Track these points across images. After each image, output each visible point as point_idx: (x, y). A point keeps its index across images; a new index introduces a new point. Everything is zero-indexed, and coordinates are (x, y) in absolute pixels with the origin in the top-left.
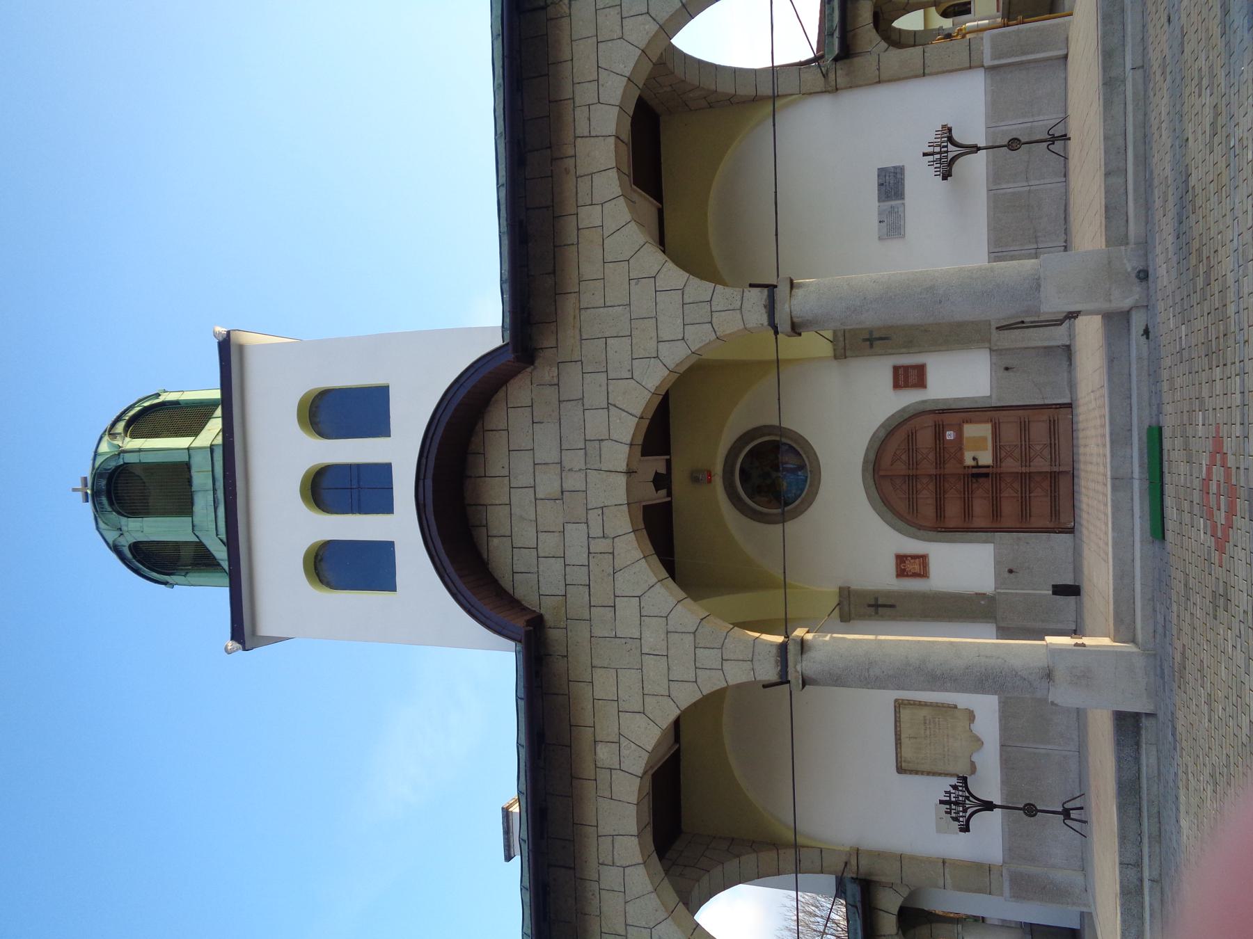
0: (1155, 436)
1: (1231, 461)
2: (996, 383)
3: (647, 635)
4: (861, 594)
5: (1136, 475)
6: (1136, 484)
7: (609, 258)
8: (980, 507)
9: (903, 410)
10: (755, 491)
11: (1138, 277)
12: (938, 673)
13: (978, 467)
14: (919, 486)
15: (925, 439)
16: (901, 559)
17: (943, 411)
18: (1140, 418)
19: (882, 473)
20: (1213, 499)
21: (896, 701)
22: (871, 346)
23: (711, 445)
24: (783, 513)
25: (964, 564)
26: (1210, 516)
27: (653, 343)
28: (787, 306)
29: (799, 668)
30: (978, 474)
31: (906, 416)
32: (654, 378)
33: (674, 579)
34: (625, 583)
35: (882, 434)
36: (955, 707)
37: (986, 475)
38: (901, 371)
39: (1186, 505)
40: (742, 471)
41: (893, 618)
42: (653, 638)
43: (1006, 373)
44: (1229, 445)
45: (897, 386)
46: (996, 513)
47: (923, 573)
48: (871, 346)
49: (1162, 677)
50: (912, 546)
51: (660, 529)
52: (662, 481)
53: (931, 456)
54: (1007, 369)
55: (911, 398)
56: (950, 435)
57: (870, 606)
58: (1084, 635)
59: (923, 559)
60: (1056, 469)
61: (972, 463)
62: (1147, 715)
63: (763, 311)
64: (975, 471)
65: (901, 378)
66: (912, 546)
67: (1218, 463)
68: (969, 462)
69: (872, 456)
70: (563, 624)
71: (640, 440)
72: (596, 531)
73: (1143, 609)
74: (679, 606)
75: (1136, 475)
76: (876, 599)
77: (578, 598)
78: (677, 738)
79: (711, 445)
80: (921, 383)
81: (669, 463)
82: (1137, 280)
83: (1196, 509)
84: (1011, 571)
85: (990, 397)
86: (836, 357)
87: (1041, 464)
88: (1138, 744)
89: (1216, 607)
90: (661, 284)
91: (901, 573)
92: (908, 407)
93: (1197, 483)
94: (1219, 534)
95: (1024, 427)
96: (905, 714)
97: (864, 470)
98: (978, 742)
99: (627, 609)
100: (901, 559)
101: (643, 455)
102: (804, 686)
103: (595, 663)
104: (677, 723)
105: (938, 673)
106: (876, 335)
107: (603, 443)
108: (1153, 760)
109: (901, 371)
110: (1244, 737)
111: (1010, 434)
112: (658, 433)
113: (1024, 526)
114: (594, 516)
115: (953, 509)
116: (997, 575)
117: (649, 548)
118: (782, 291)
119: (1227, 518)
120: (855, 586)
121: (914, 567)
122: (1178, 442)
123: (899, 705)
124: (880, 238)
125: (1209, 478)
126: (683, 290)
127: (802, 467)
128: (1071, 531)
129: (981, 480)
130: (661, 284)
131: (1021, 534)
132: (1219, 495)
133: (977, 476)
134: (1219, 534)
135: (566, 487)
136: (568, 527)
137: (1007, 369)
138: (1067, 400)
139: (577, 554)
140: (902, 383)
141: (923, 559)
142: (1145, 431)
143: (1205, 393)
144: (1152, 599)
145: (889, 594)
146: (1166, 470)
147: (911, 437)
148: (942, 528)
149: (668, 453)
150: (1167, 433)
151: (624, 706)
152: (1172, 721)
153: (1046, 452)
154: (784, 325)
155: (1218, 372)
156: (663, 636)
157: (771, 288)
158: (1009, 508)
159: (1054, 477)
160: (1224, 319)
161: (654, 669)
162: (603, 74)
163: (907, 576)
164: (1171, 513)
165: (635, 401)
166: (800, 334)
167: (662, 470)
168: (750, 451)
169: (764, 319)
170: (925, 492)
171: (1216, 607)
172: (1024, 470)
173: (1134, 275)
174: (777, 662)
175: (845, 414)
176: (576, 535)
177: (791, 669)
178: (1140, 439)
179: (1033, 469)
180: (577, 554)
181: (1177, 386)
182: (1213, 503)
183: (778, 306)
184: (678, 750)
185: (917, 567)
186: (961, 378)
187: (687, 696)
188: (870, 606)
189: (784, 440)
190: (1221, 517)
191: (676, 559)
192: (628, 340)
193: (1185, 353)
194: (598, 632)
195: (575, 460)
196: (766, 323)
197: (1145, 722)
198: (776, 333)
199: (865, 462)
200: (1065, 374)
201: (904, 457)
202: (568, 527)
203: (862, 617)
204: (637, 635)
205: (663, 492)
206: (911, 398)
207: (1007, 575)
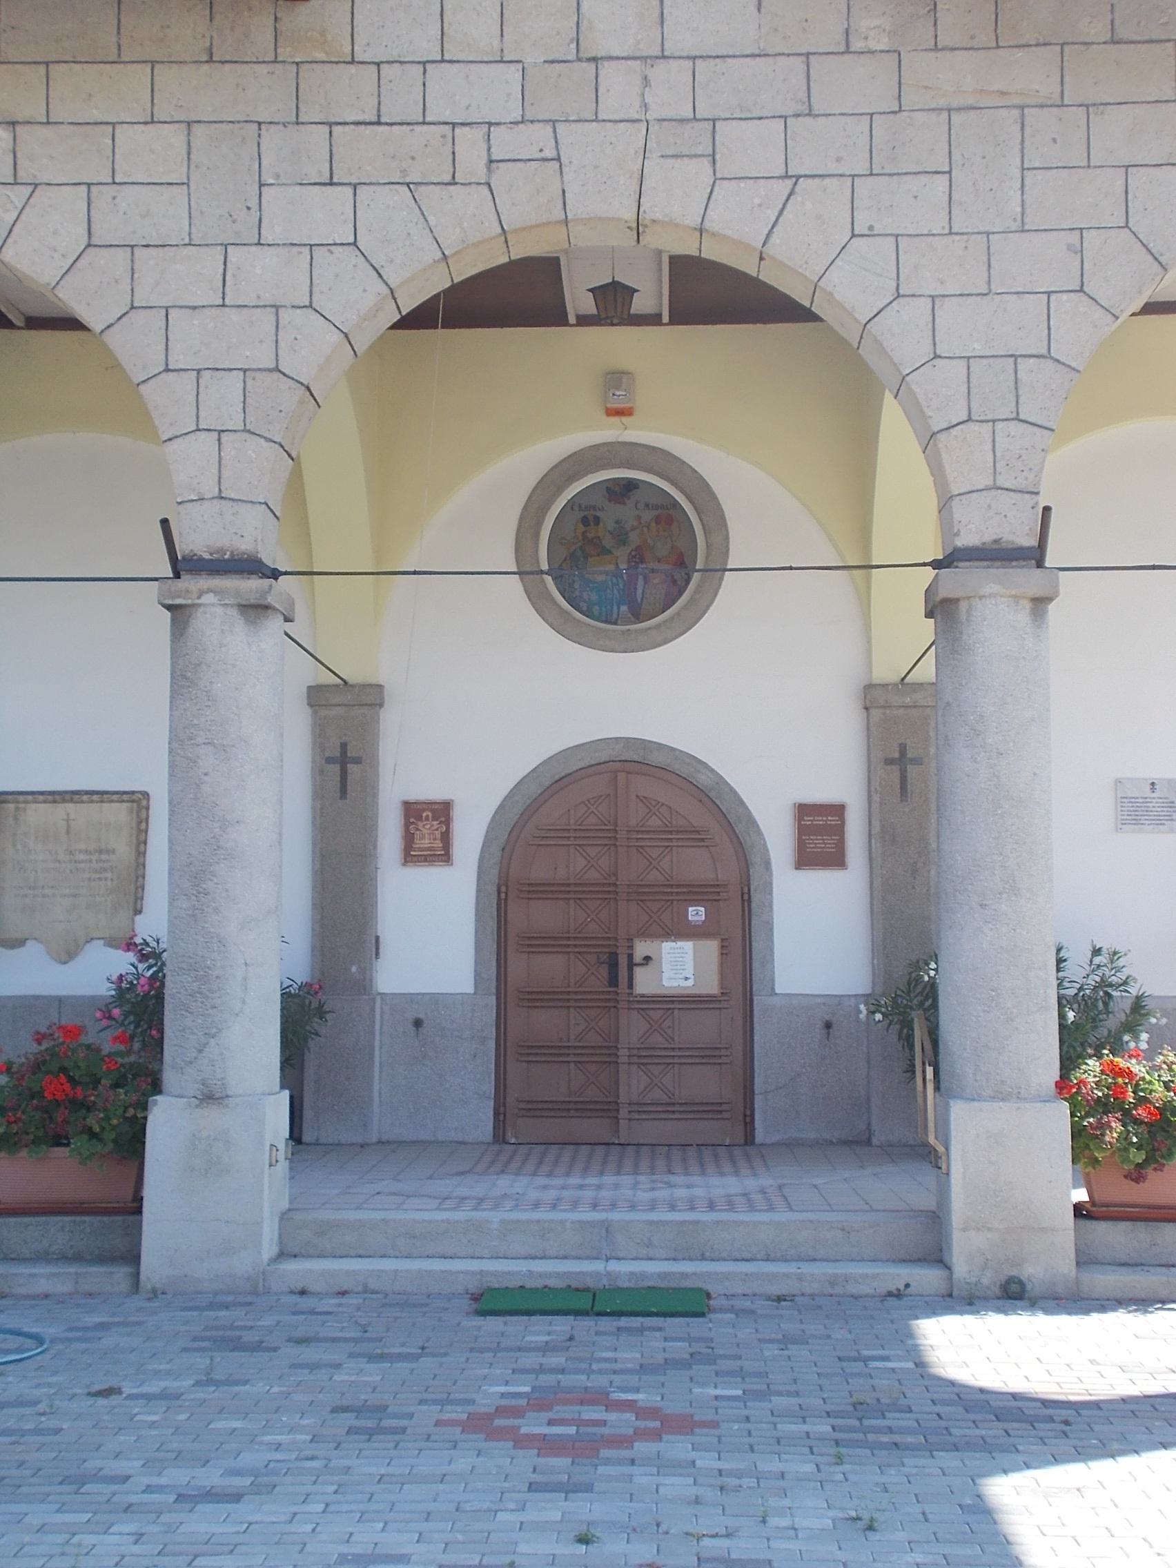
0: (689, 1303)
1: (641, 1448)
2: (802, 1004)
3: (270, 258)
4: (369, 731)
5: (614, 1266)
6: (598, 1266)
7: (1137, 177)
8: (552, 968)
9: (752, 823)
10: (584, 515)
11: (1011, 1280)
12: (209, 886)
13: (631, 965)
14: (593, 851)
15: (695, 865)
16: (442, 812)
17: (746, 899)
18: (727, 1276)
19: (621, 777)
20: (568, 1412)
21: (146, 795)
22: (889, 762)
23: (699, 414)
24: (542, 572)
25: (431, 935)
26: (540, 1402)
27: (932, 288)
28: (994, 588)
29: (209, 598)
30: (617, 966)
31: (740, 829)
32: (849, 287)
33: (395, 326)
34: (385, 211)
35: (703, 779)
36: (138, 911)
37: (613, 981)
38: (833, 820)
39: (557, 1360)
40: (630, 486)
41: (318, 794)
42: (261, 272)
43: (820, 1025)
44: (677, 1447)
45: (804, 811)
46: (535, 998)
47: (411, 855)
48: (889, 762)
49: (212, 1306)
50: (469, 836)
51: (509, 297)
52: (613, 304)
53: (654, 876)
54: (828, 1025)
55: (778, 837)
56: (696, 914)
57: (344, 746)
58: (291, 1161)
59: (444, 855)
60: (623, 1113)
61: (638, 957)
62: (137, 1275)
63: (988, 537)
64: (623, 961)
65: (820, 821)
66: (469, 836)
67: (641, 1424)
68: (642, 948)
69: (657, 758)
70: (284, 53)
71: (711, 252)
72: (506, 142)
73: (347, 1272)
74: (336, 337)
75: (614, 1266)
76: (358, 761)
77: (348, 93)
78: (36, 323)
79: (699, 414)
80: (806, 859)
81: (653, 320)
82: (1003, 1278)
83: (547, 1380)
84: (418, 1023)
85: (773, 993)
86: (869, 688)
87: (633, 1084)
88: (77, 1258)
89: (358, 1410)
90: (1062, 302)
91: (413, 812)
92: (759, 833)
93: (601, 1381)
94: (499, 1422)
95: (709, 1055)
96: (119, 813)
97: (628, 742)
98: (68, 953)
99: (325, 214)
100: (442, 812)
101: (675, 260)
102: (169, 607)
103: (197, 129)
104: (72, 324)
105: (209, 886)
106: (912, 771)
107: (705, 163)
108: (43, 1286)
109: (833, 820)
110: (98, 1463)
111: (698, 1029)
112: (714, 295)
113: (510, 1050)
114: (537, 139)
115: (545, 916)
116: (411, 998)
117: (465, 270)
118: (1027, 580)
119: (531, 1438)
120: (390, 720)
121: (426, 838)
122: (680, 1349)
123: (138, 801)
124: (1118, 782)
125: (612, 1405)
126: (1047, 356)
127: (638, 615)
128: (499, 1137)
129: (604, 971)
130: (1062, 302)
131: (492, 1044)
132: (579, 1423)
133: (613, 964)
134: (499, 1422)
135: (607, 68)
136: (514, 73)
137: (828, 1025)
138: (759, 1136)
139: (453, 93)
140: (808, 821)
141: (444, 855)
142: (699, 1284)
143: (779, 1402)
144: (366, 1290)
145: (370, 789)
146: (624, 1322)
147: (696, 837)
148: (510, 898)
149: (673, 322)
150: (695, 1326)
151: (103, 196)
152: (124, 1324)
153: (657, 1095)
154: (954, 582)
155: (823, 1428)
156: (267, 298)
157: (1036, 556)
158: (546, 1022)
159: (608, 1109)
160: (930, 1449)
161: (193, 276)
162: (789, 182)
163: (407, 824)
164: (540, 1330)
165: (795, 252)
166: (929, 614)
167: (641, 304)
168: (676, 504)
169: (968, 539)
170: (581, 862)
171: (358, 1410)
172: (623, 1053)
173: (1014, 1273)
174: (221, 551)
175: (497, 702)
176: (495, 92)
177: (205, 582)
178: (684, 1276)
179: (623, 1069)
180: (453, 93)
181: (793, 1350)
182: (560, 1411)
183: (996, 572)
184: (9, 325)
185: (426, 843)
186: (817, 937)
187: (136, 346)
188: (344, 746)
189: (696, 577)
190: (533, 1425)
191: (440, 331)
192: (940, 225)
193: (857, 1367)
194: (272, 140)
195: (669, 92)
196: (960, 542)
197: (121, 1273)
198: (936, 564)
199: (645, 744)
200: (813, 1135)
201: (654, 822)
202: (514, 73)
203: (320, 732)
204: (267, 237)
205: (588, 305)
206: (778, 837)
207: (410, 1016)
